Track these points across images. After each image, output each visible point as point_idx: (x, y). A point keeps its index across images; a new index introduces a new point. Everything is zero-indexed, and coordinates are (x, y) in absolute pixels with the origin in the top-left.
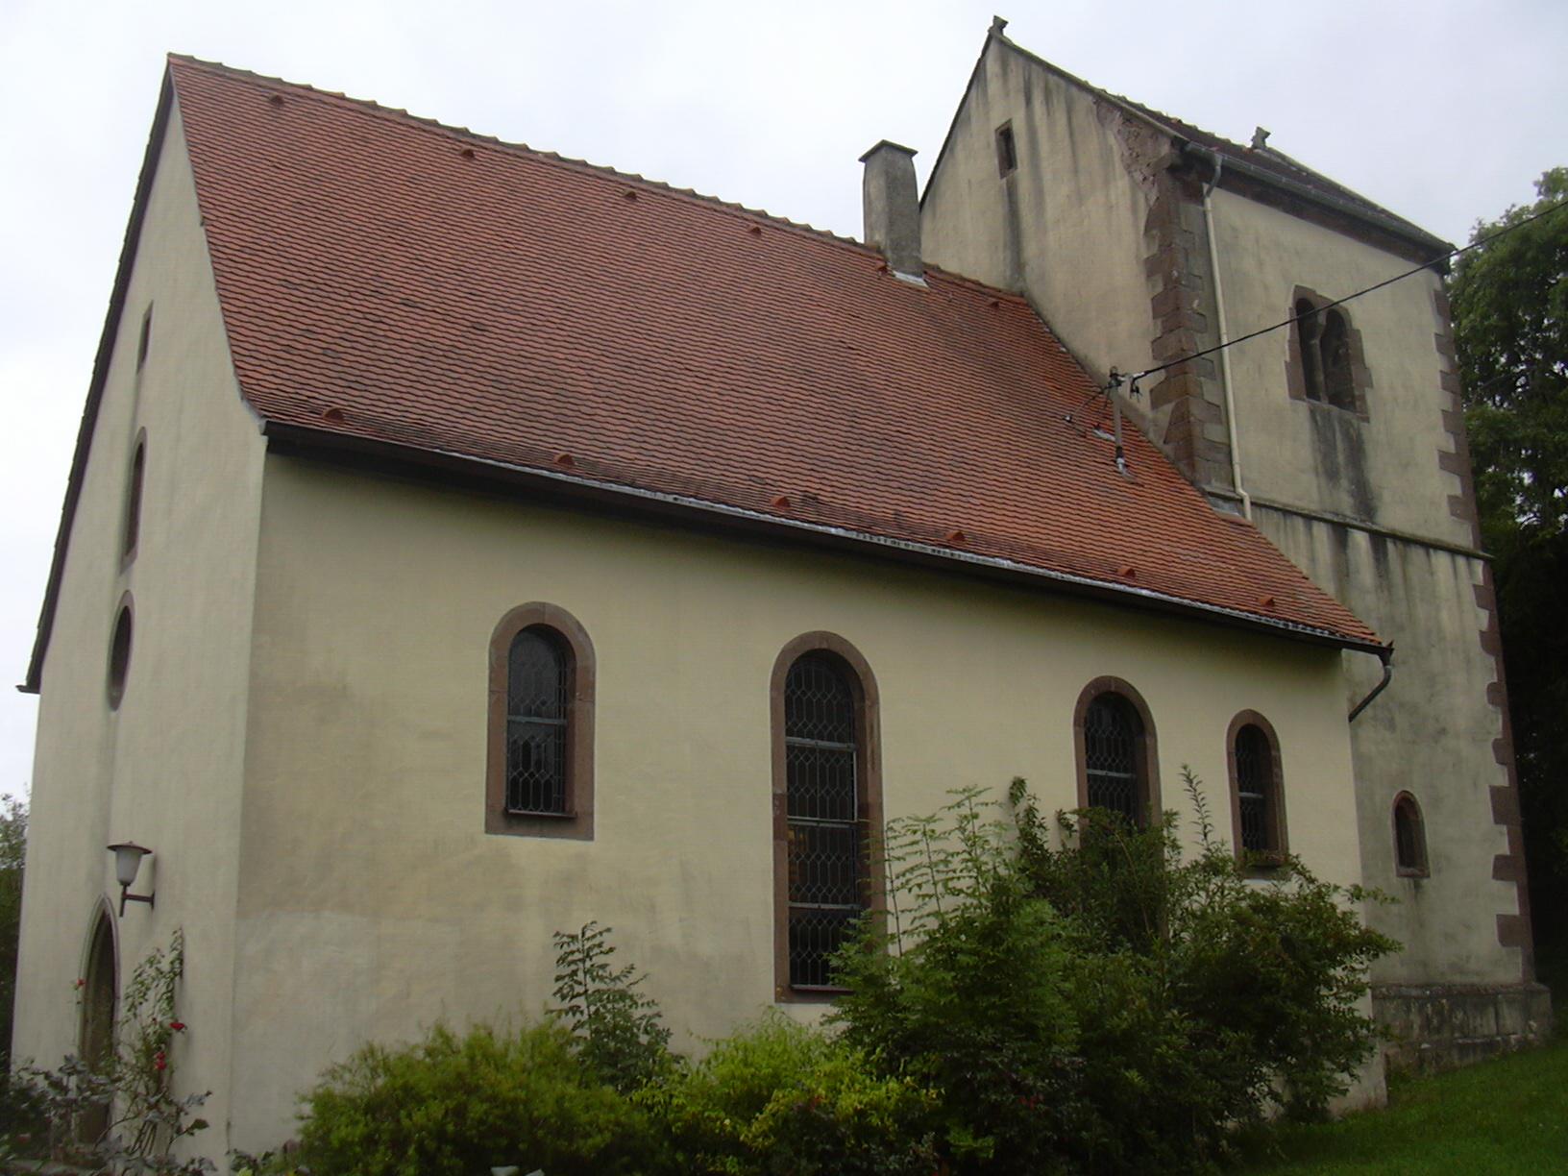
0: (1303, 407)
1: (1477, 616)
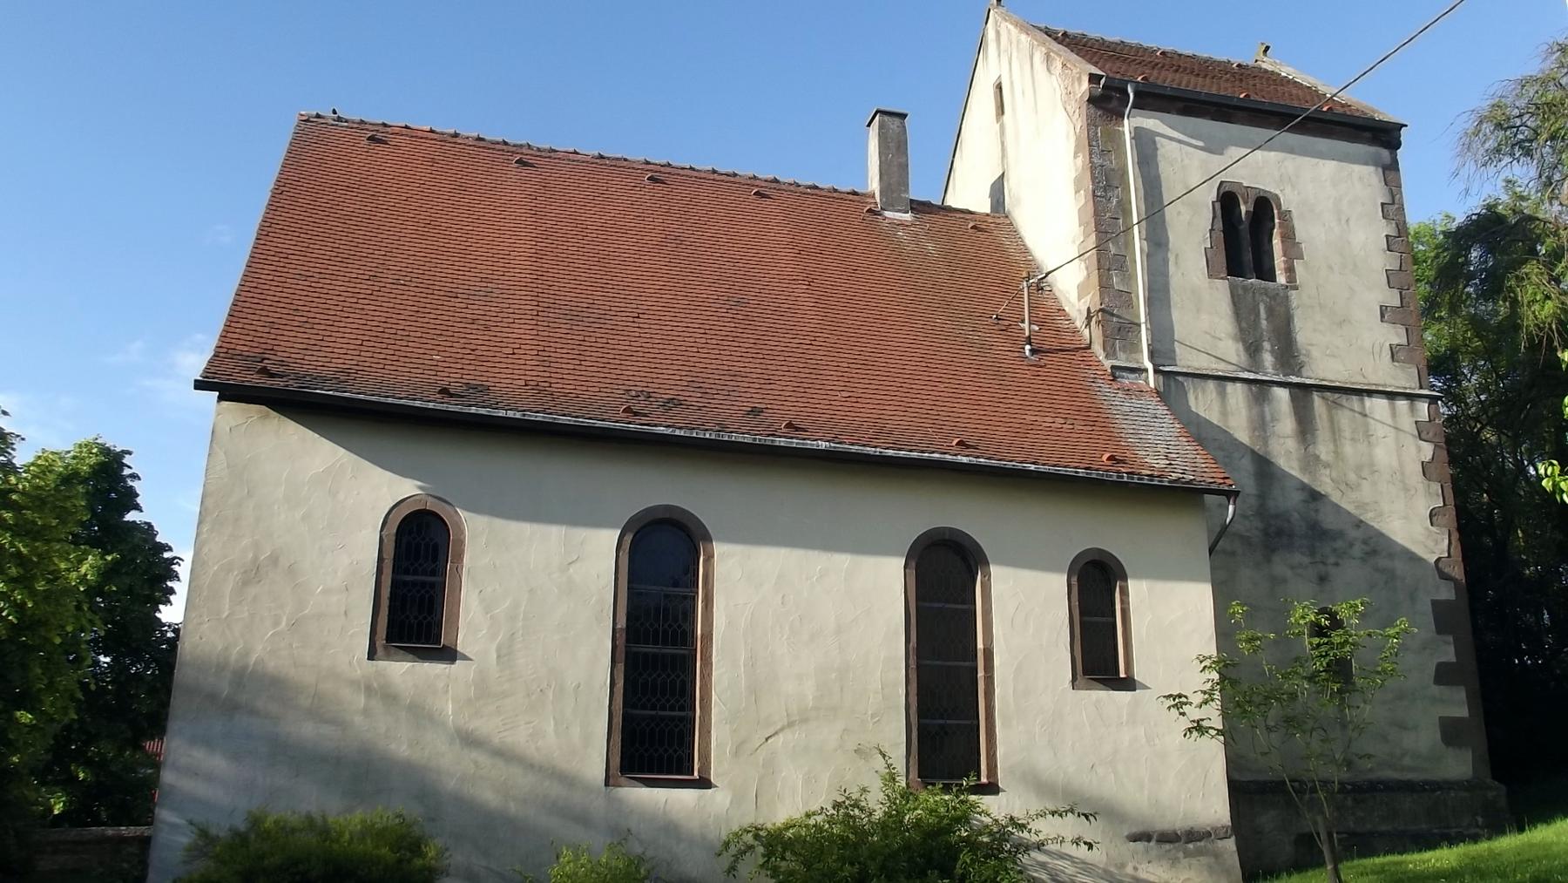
0: (1222, 287)
1: (1419, 449)
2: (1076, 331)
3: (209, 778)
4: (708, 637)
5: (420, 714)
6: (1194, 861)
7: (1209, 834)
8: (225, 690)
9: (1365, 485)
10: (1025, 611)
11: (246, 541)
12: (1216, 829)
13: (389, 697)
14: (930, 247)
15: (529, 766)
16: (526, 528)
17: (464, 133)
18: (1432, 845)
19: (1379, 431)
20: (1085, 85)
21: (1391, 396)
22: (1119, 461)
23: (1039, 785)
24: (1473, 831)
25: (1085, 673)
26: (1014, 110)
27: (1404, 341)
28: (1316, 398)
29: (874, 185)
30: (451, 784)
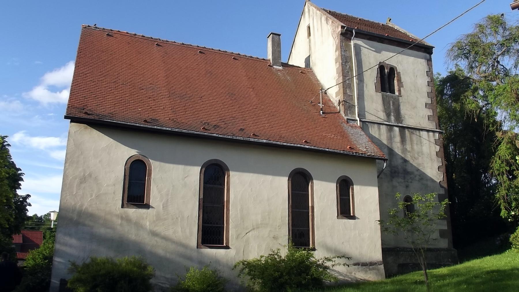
0: (380, 95)
1: (436, 148)
2: (335, 107)
3: (71, 246)
4: (228, 201)
5: (138, 225)
6: (372, 271)
7: (376, 263)
8: (75, 217)
9: (420, 158)
10: (323, 194)
11: (81, 169)
12: (378, 262)
13: (127, 219)
14: (288, 78)
15: (173, 242)
16: (171, 166)
17: (138, 34)
18: (438, 268)
19: (425, 142)
20: (340, 29)
21: (428, 131)
22: (352, 149)
23: (328, 249)
24: (447, 263)
25: (341, 214)
26: (314, 35)
27: (432, 114)
28: (406, 131)
29: (270, 57)
30: (149, 248)
